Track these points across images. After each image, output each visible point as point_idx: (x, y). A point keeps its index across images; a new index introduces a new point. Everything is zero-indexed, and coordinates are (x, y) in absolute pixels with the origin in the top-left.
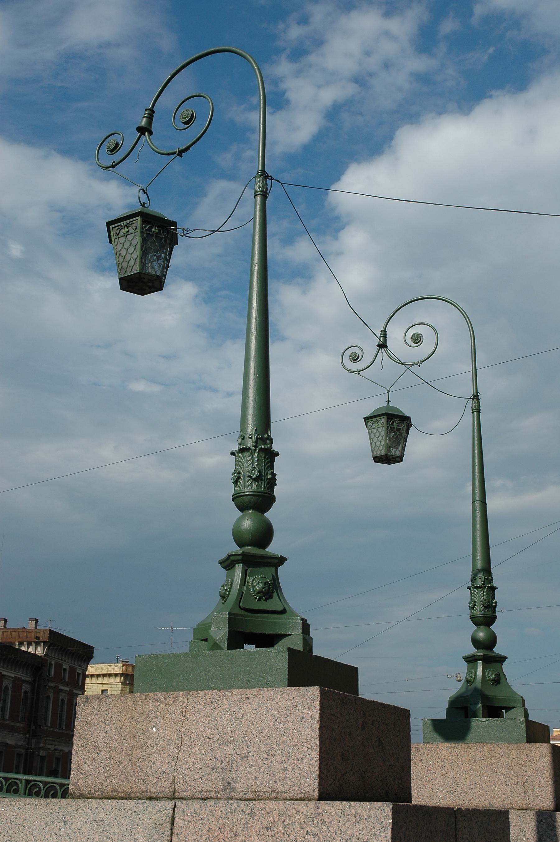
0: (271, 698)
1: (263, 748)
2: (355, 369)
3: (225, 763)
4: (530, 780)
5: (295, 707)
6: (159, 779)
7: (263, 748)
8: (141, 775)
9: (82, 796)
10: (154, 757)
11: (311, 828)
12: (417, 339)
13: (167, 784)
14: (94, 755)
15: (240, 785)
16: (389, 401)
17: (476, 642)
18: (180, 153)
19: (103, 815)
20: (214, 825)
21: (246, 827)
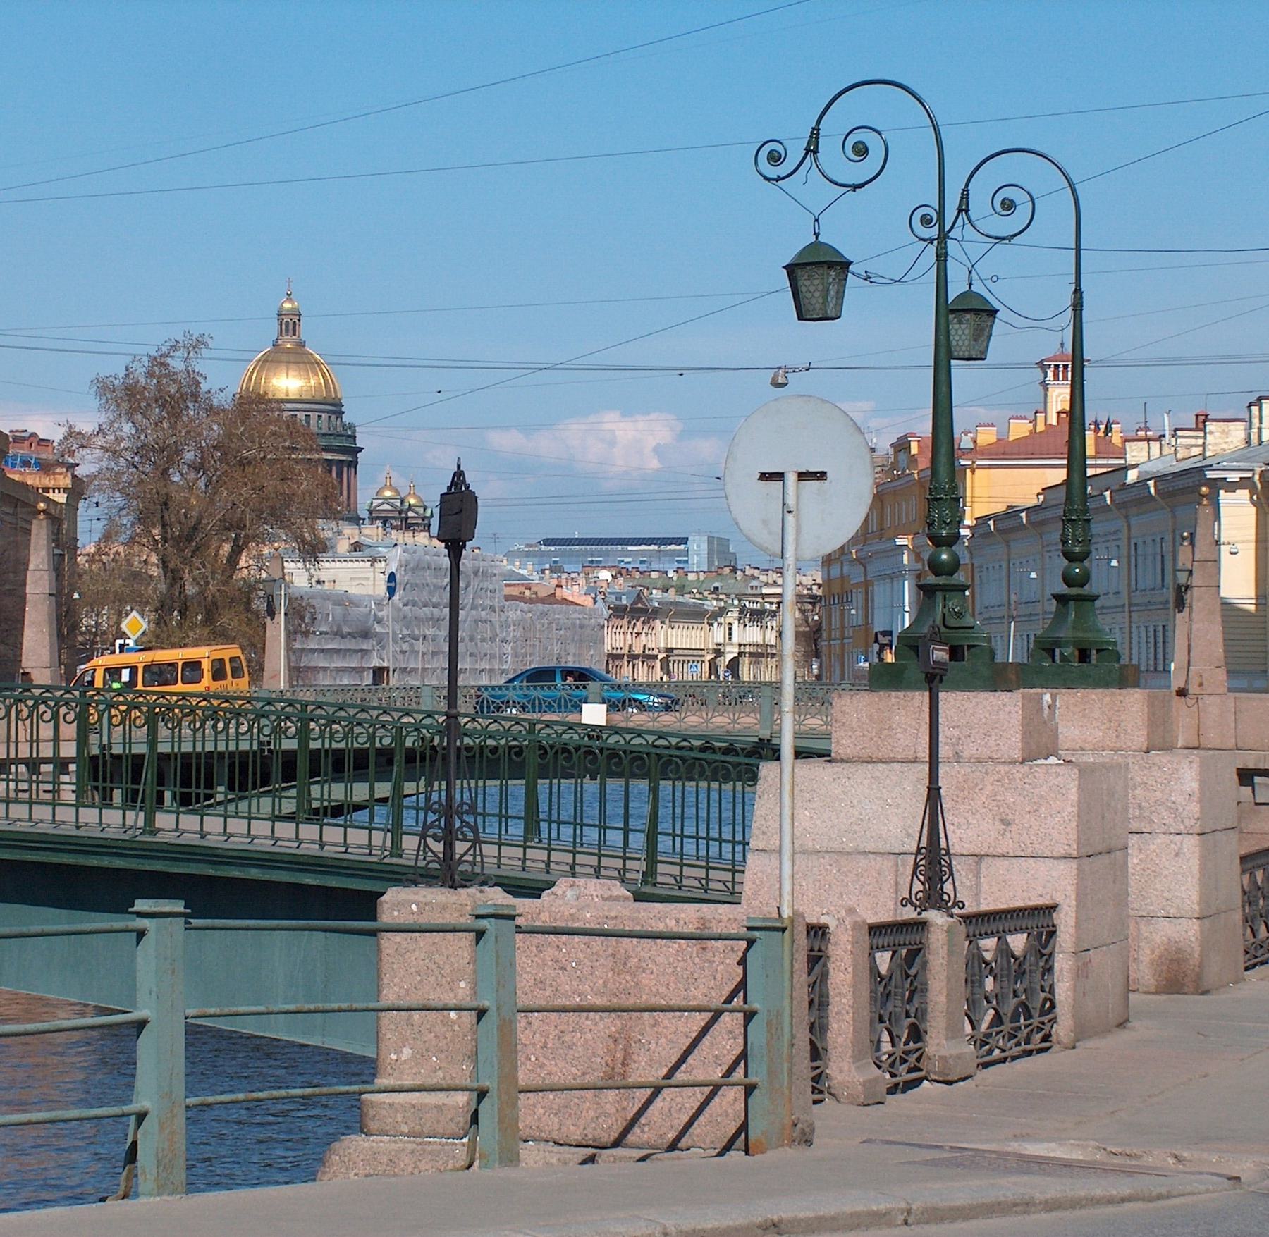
0: (986, 699)
1: (981, 731)
2: (926, 236)
3: (954, 740)
4: (1122, 724)
5: (1004, 705)
6: (904, 750)
7: (981, 731)
8: (889, 748)
9: (842, 761)
10: (899, 736)
11: (1026, 780)
12: (1009, 205)
13: (912, 753)
14: (850, 734)
15: (966, 754)
16: (970, 285)
17: (1068, 580)
18: (855, 187)
19: (878, 774)
20: (960, 779)
21: (983, 780)
